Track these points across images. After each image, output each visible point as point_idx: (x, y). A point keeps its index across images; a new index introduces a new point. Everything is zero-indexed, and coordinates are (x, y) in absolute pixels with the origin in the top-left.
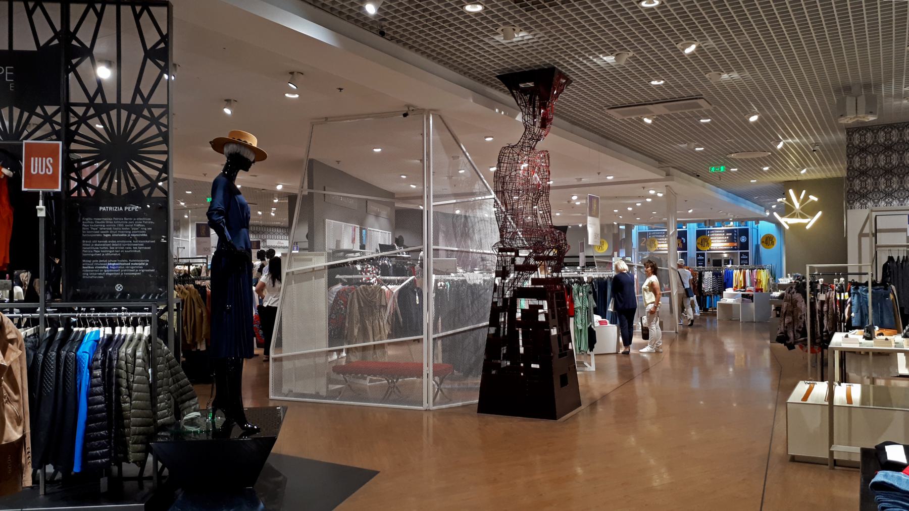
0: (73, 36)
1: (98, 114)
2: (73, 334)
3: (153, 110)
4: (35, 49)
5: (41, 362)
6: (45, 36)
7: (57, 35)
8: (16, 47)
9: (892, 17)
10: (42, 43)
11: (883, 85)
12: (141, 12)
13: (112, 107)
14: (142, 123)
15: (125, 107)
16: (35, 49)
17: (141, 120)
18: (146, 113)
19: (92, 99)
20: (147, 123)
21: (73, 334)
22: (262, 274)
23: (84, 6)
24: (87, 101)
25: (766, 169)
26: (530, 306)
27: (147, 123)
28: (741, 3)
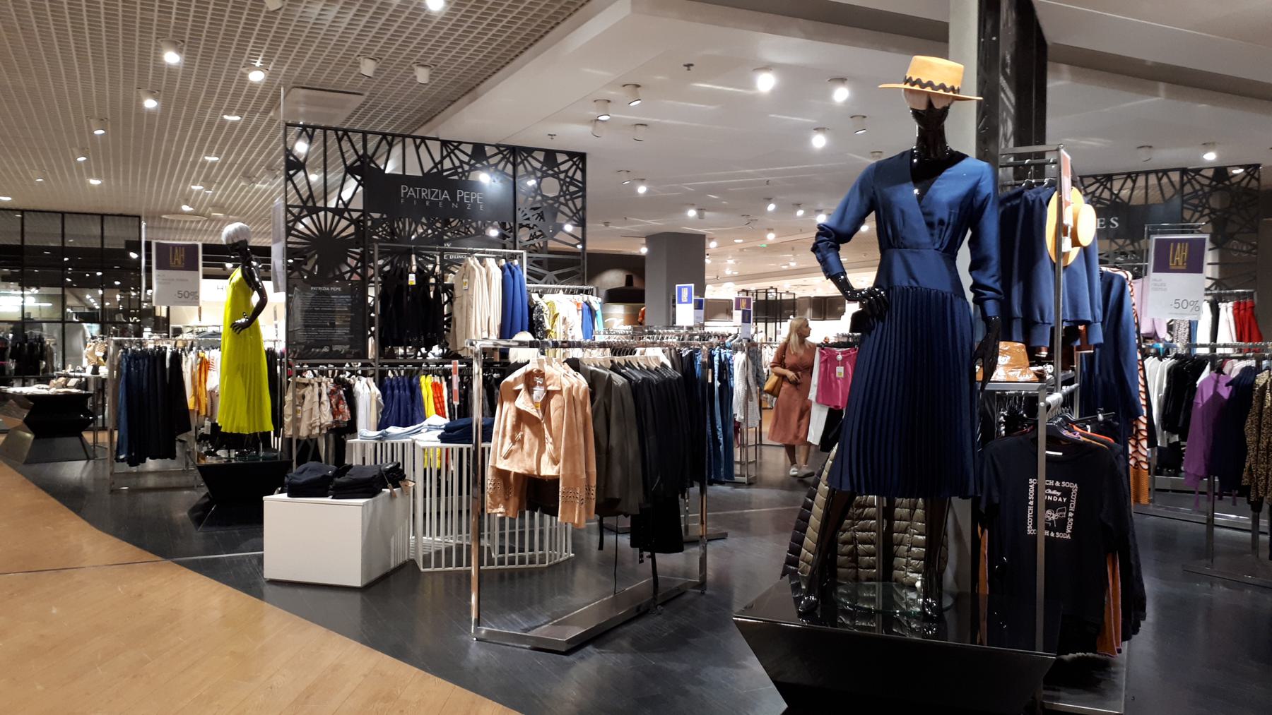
0: (372, 159)
1: (310, 215)
2: (1015, 272)
3: (352, 213)
4: (421, 175)
5: (1015, 279)
6: (428, 165)
7: (359, 158)
8: (407, 173)
9: (248, 14)
10: (426, 171)
11: (258, 114)
12: (420, 144)
13: (320, 209)
14: (344, 223)
15: (331, 210)
16: (421, 175)
17: (343, 220)
18: (346, 215)
19: (305, 203)
20: (348, 223)
21: (1015, 272)
22: (28, 462)
23: (469, 153)
24: (350, 207)
25: (117, 283)
26: (1019, 281)
27: (348, 223)
28: (102, 3)
